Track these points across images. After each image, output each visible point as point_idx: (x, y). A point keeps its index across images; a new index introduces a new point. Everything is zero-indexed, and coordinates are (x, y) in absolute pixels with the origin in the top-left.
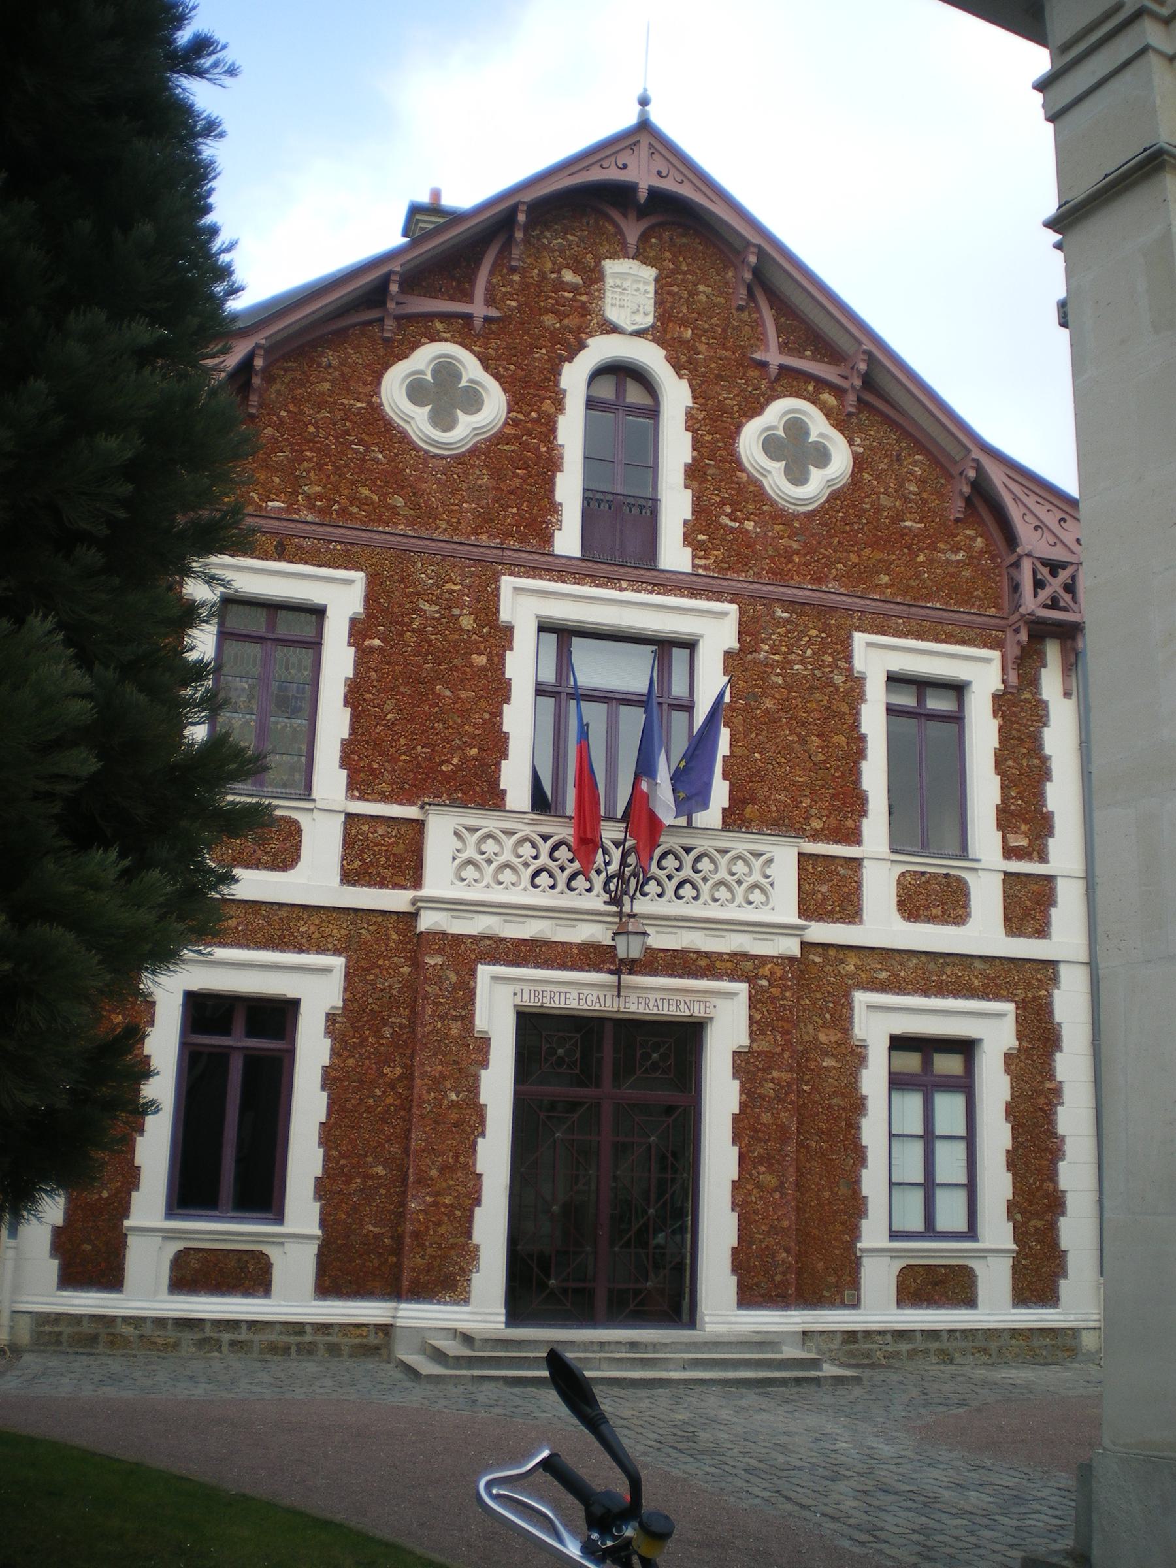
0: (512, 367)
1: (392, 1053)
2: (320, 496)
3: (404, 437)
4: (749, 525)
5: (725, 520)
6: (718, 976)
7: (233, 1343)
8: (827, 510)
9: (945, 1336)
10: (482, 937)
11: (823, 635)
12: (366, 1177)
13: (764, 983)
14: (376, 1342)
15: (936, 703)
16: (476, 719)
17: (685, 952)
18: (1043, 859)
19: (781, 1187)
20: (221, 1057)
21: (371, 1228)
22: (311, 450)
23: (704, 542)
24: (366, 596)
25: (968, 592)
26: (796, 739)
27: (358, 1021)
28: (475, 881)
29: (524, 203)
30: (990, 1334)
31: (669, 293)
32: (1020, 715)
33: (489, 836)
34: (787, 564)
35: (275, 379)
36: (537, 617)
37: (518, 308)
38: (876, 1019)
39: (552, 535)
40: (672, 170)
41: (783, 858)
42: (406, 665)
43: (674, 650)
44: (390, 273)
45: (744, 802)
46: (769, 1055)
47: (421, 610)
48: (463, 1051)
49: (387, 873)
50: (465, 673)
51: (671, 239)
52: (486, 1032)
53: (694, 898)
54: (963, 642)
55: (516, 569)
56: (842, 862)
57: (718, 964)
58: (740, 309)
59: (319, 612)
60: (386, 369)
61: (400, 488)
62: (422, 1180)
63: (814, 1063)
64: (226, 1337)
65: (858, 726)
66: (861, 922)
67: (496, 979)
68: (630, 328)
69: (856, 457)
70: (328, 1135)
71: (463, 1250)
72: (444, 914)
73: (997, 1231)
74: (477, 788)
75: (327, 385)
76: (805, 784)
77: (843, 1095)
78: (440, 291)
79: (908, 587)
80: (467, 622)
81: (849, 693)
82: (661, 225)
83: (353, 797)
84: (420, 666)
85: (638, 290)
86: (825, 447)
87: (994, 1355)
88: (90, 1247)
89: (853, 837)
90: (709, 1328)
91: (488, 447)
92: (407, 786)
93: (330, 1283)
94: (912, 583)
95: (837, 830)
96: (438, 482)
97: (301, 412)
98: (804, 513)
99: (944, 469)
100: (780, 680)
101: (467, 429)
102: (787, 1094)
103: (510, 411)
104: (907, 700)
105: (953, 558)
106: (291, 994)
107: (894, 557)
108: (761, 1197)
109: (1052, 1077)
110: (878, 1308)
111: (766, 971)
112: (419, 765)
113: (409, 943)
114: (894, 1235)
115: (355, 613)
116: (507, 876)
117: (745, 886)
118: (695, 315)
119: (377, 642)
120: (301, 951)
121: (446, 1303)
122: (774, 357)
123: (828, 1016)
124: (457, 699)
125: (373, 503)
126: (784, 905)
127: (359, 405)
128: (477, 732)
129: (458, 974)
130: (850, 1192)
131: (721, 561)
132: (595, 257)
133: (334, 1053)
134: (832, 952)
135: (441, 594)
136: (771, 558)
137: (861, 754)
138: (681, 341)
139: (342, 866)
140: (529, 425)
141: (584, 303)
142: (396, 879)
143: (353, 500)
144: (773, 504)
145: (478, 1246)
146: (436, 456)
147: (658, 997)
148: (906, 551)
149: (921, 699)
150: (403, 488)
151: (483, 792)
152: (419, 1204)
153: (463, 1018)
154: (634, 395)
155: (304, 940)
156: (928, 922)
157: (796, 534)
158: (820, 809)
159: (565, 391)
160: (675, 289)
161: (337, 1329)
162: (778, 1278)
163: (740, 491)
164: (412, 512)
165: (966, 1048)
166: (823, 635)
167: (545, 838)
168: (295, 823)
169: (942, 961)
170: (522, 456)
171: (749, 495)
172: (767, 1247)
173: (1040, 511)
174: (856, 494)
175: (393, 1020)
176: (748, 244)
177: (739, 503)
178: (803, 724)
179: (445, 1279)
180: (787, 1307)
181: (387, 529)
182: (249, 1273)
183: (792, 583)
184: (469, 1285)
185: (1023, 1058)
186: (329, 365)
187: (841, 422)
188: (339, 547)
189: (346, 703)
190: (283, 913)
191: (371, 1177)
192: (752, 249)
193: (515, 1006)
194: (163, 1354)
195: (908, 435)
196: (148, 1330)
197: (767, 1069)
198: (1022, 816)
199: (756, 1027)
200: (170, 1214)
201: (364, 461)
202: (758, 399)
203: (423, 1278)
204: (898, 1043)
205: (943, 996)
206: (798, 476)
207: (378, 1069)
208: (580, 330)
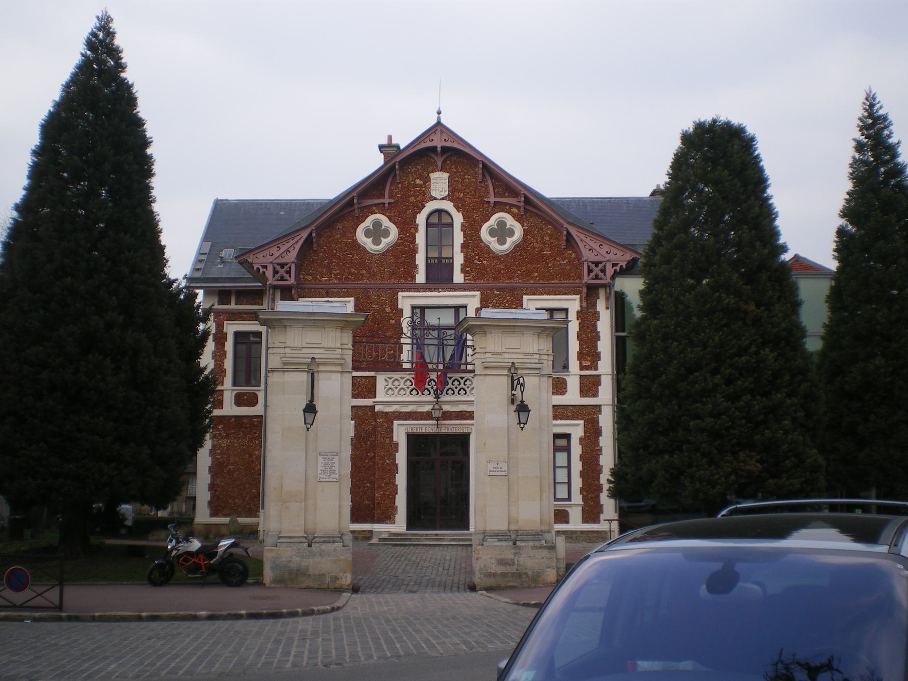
2: (338, 274)
3: (365, 249)
4: (485, 262)
5: (476, 262)
10: (395, 412)
18: (596, 369)
30: (572, 532)
32: (588, 318)
54: (566, 294)
62: (380, 487)
67: (399, 425)
69: (524, 230)
73: (577, 498)
79: (545, 276)
80: (388, 310)
101: (385, 242)
116: (402, 392)
133: (352, 450)
138: (459, 198)
143: (349, 273)
163: (481, 250)
170: (404, 250)
171: (486, 250)
173: (592, 244)
176: (478, 161)
179: (387, 516)
187: (518, 219)
195: (545, 219)
198: (588, 354)
206: (502, 242)
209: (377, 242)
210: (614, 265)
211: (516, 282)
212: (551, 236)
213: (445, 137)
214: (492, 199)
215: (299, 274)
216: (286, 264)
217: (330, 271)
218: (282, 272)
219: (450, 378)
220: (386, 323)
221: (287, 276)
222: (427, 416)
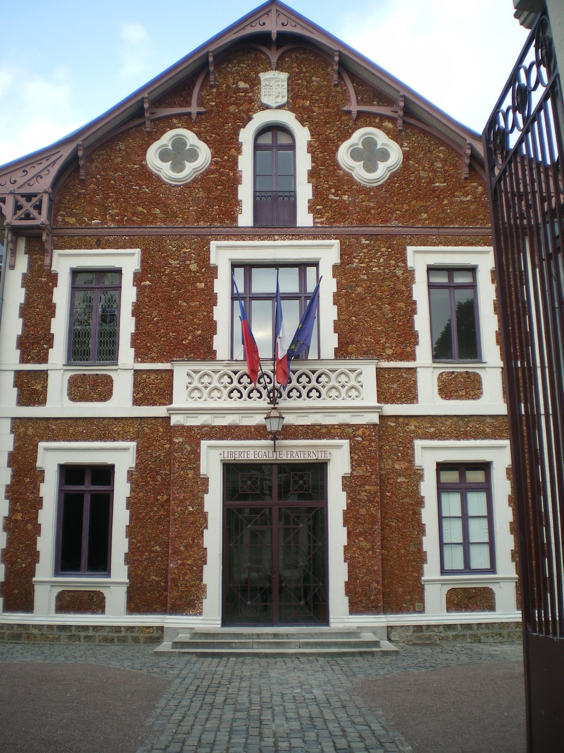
0: (214, 135)
1: (162, 489)
2: (118, 214)
3: (159, 178)
4: (345, 197)
5: (331, 196)
6: (333, 437)
7: (86, 637)
8: (389, 184)
9: (475, 627)
10: (203, 426)
11: (390, 250)
12: (151, 552)
13: (359, 439)
14: (157, 635)
15: (459, 279)
16: (200, 315)
17: (313, 426)
19: (372, 548)
20: (80, 496)
21: (154, 578)
22: (112, 192)
23: (320, 209)
24: (141, 260)
25: (475, 217)
26: (375, 307)
27: (144, 473)
28: (337, 397)
29: (210, 52)
31: (296, 84)
33: (343, 373)
34: (367, 215)
35: (94, 161)
36: (230, 260)
37: (216, 105)
38: (427, 455)
39: (237, 217)
40: (290, 21)
41: (368, 371)
42: (163, 292)
43: (308, 268)
44: (143, 98)
45: (347, 344)
46: (363, 477)
47: (170, 264)
48: (195, 485)
49: (156, 398)
50: (193, 293)
51: (296, 56)
52: (206, 475)
53: (258, 398)
54: (472, 244)
55: (217, 237)
56: (405, 371)
57: (333, 431)
58: (336, 86)
59: (119, 272)
60: (149, 147)
61: (157, 205)
62: (176, 552)
63: (392, 480)
64: (82, 634)
65: (411, 297)
66: (417, 402)
67: (210, 447)
68: (274, 105)
69: (404, 153)
70: (130, 532)
71: (198, 587)
72: (182, 416)
73: (507, 568)
74: (202, 351)
75: (120, 159)
76: (382, 331)
77: (410, 497)
78: (175, 103)
79: (438, 219)
80: (194, 267)
81: (405, 279)
82: (290, 50)
83: (138, 362)
84: (170, 293)
85: (278, 85)
86: (386, 150)
87: (506, 637)
88: (17, 591)
89: (412, 356)
90: (332, 625)
91: (202, 178)
92: (165, 353)
93: (134, 606)
94: (441, 216)
95: (401, 354)
96: (177, 198)
97: (107, 174)
98: (376, 187)
99: (456, 152)
100: (365, 277)
101: (191, 169)
102: (374, 498)
103: (213, 157)
104: (442, 279)
105: (465, 199)
106: (110, 462)
107: (429, 203)
108: (361, 554)
110: (435, 611)
111: (360, 432)
112: (171, 342)
113: (169, 432)
114: (443, 571)
115: (135, 270)
116: (216, 394)
117: (346, 388)
118: (311, 93)
119: (148, 283)
120: (114, 440)
121: (190, 615)
122: (354, 107)
123: (400, 454)
125: (144, 214)
126: (369, 396)
127: (136, 166)
128: (200, 322)
129: (191, 446)
130: (416, 549)
131: (330, 218)
132: (255, 73)
133: (132, 490)
134: (401, 420)
135: (180, 255)
136: (359, 213)
137: (414, 311)
138: (304, 108)
139: (134, 396)
140: (224, 163)
141: (250, 97)
142: (161, 401)
143: (134, 214)
144: (358, 184)
145: (206, 585)
146: (176, 186)
147: (298, 450)
148: (436, 199)
149: (451, 278)
150: (159, 204)
151: (205, 352)
152: (175, 565)
153: (194, 468)
154: (283, 139)
155: (116, 435)
156: (457, 399)
157: (372, 198)
158: (391, 343)
159: (242, 143)
160: (300, 82)
161: (137, 629)
162: (372, 597)
164: (164, 216)
165: (485, 467)
166: (390, 250)
167: (235, 373)
168: (110, 377)
169: (466, 420)
170: (220, 182)
171: (346, 181)
172: (366, 581)
174: (406, 173)
175: (162, 472)
177: (339, 187)
178: (380, 299)
179: (190, 603)
180: (378, 613)
181: (151, 226)
182: (94, 602)
183: (371, 225)
184: (202, 606)
186: (120, 149)
187: (395, 136)
188: (127, 238)
189: (133, 315)
190: (105, 422)
191: (153, 552)
192: (335, 53)
193: (221, 460)
194: (52, 643)
195: (435, 137)
196: (45, 631)
197: (363, 485)
199: (355, 463)
200: (57, 574)
201: (139, 193)
202: (348, 131)
203: (178, 602)
204: (442, 467)
205: (468, 439)
206: (371, 167)
207: (155, 497)
208: (249, 111)
209: (178, 167)
211: (395, 227)
212: (444, 161)
213: (284, 20)
214: (354, 107)
215: (56, 216)
216: (35, 195)
217: (104, 210)
218: (28, 206)
219: (294, 372)
220: (189, 287)
221: (34, 213)
222: (259, 432)
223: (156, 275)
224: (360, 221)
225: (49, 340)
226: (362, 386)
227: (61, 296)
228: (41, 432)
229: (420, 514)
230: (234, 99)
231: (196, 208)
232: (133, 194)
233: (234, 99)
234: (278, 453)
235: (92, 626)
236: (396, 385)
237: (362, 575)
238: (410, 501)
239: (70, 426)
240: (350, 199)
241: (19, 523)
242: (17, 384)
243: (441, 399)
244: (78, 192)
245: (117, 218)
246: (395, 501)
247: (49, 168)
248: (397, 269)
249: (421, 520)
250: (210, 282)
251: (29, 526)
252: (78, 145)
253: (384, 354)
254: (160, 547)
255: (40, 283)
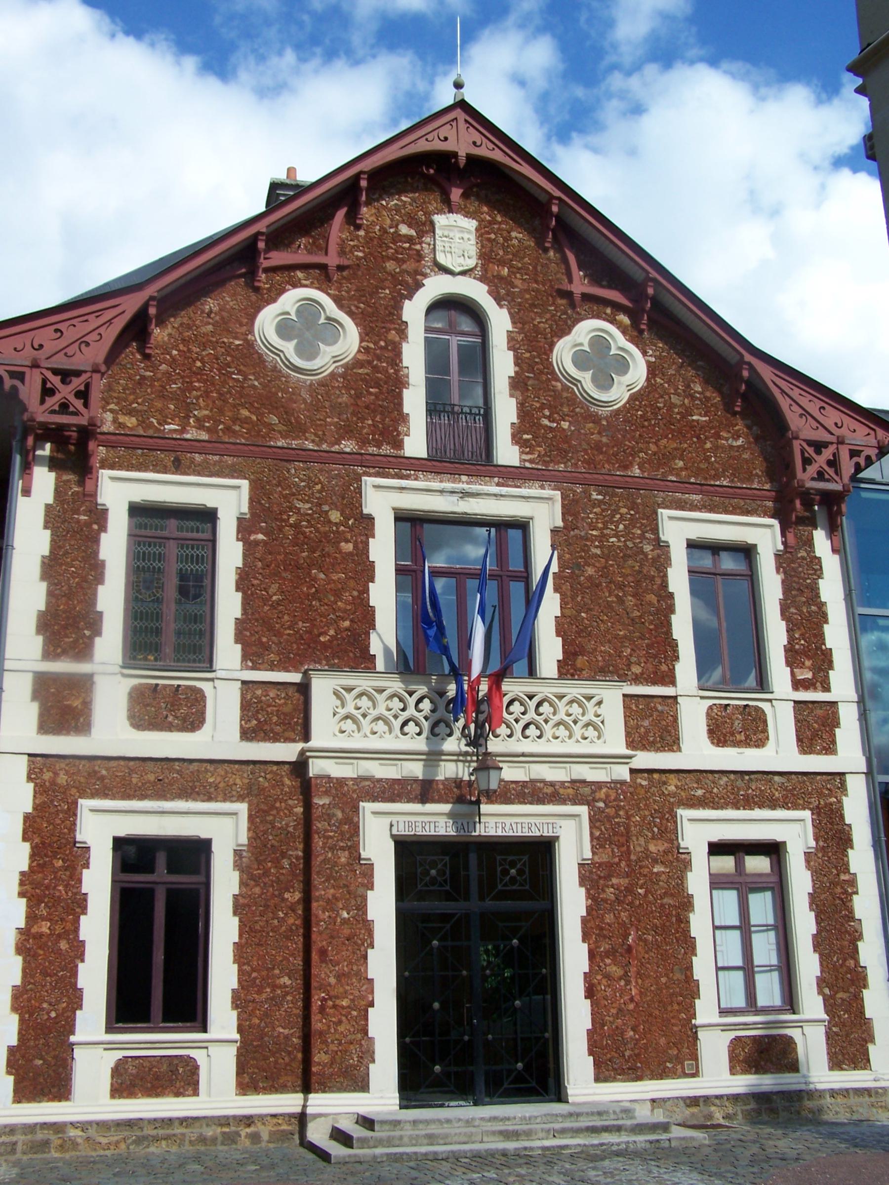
0: (362, 305)
1: (291, 881)
2: (208, 418)
4: (565, 425)
5: (546, 422)
8: (628, 409)
11: (632, 512)
12: (274, 987)
13: (601, 805)
16: (346, 596)
18: (827, 689)
19: (625, 976)
21: (282, 1030)
22: (199, 381)
26: (615, 599)
36: (394, 509)
38: (697, 830)
44: (259, 233)
45: (575, 654)
46: (609, 865)
48: (351, 875)
65: (666, 586)
69: (649, 365)
70: (241, 953)
73: (812, 1004)
74: (351, 655)
76: (625, 637)
77: (672, 895)
81: (655, 560)
88: (41, 1062)
89: (669, 679)
92: (292, 656)
97: (189, 351)
103: (362, 341)
105: (735, 444)
107: (686, 445)
109: (847, 870)
111: (602, 794)
112: (302, 638)
114: (724, 1012)
119: (260, 537)
123: (655, 829)
124: (329, 581)
127: (237, 342)
128: (349, 607)
129: (343, 811)
133: (242, 883)
136: (585, 451)
138: (501, 278)
139: (241, 726)
142: (287, 734)
143: (235, 420)
153: (349, 848)
158: (638, 657)
160: (493, 236)
164: (285, 428)
169: (747, 777)
170: (376, 379)
172: (617, 1027)
175: (291, 853)
178: (621, 586)
182: (180, 1077)
183: (603, 471)
185: (820, 855)
191: (280, 987)
197: (608, 877)
198: (805, 653)
199: (598, 843)
200: (109, 1029)
209: (307, 350)
210: (854, 453)
216: (78, 373)
220: (329, 549)
223: (274, 525)
224: (588, 463)
225: (94, 623)
226: (602, 722)
227: (114, 547)
228: (82, 780)
229: (689, 922)
230: (392, 251)
231: (336, 420)
232: (232, 387)
233: (392, 251)
234: (482, 825)
235: (178, 1118)
236: (647, 722)
237: (611, 1019)
238: (671, 902)
239: (132, 771)
240: (573, 428)
241: (44, 939)
242: (36, 695)
243: (711, 746)
244: (140, 375)
245: (207, 424)
246: (650, 902)
247: (102, 330)
248: (644, 542)
249: (689, 931)
250: (362, 542)
251: (63, 945)
252: (152, 298)
253: (630, 673)
254: (290, 978)
255: (74, 526)
